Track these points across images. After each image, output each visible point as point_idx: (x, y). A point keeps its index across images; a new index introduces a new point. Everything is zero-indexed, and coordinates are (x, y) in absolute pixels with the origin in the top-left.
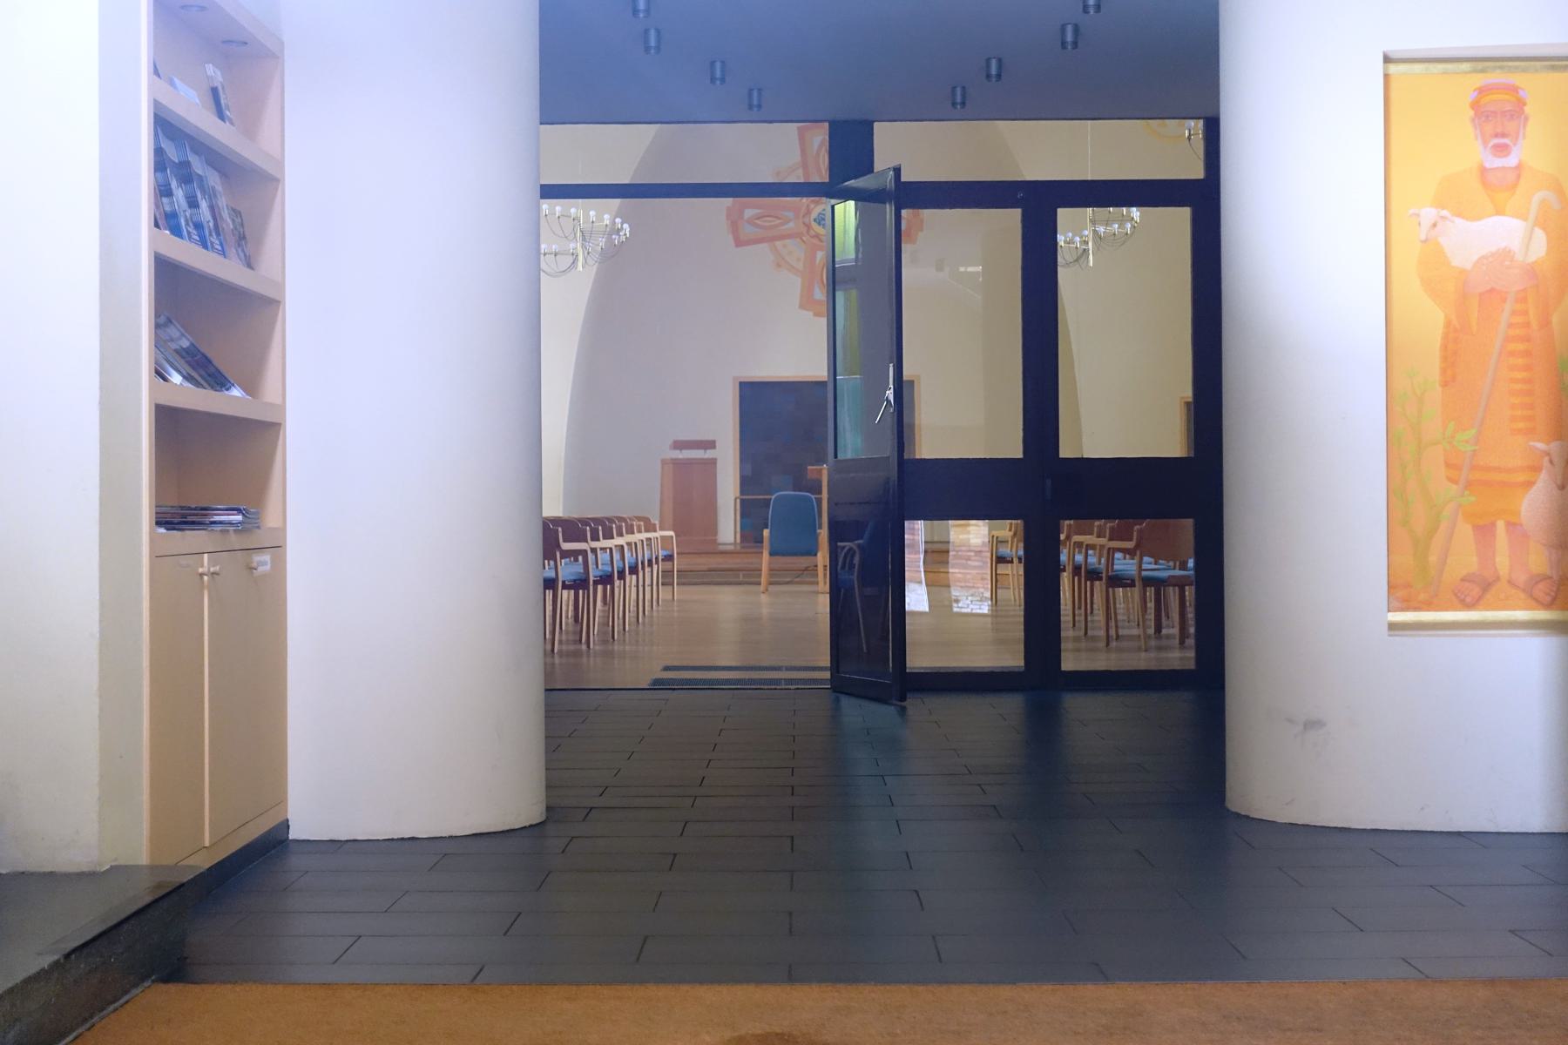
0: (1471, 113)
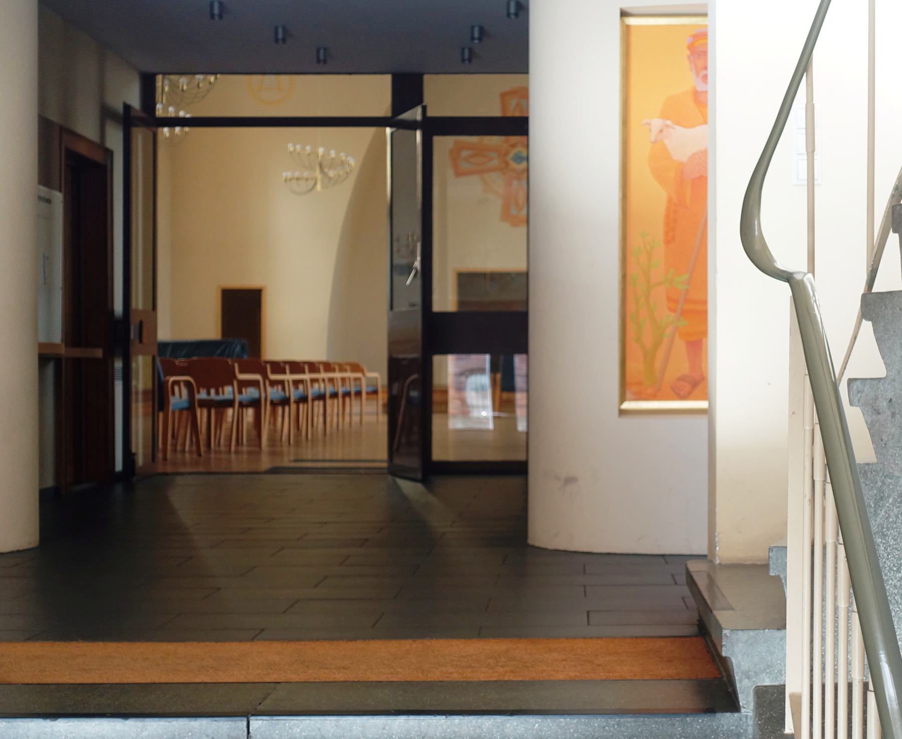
0: (688, 52)
